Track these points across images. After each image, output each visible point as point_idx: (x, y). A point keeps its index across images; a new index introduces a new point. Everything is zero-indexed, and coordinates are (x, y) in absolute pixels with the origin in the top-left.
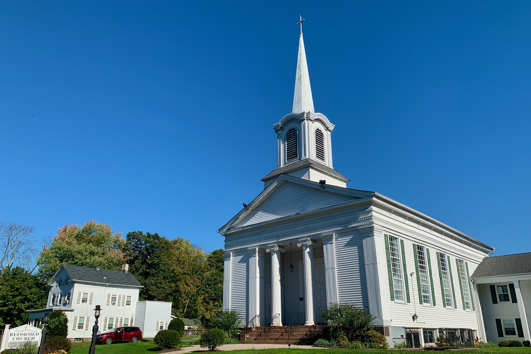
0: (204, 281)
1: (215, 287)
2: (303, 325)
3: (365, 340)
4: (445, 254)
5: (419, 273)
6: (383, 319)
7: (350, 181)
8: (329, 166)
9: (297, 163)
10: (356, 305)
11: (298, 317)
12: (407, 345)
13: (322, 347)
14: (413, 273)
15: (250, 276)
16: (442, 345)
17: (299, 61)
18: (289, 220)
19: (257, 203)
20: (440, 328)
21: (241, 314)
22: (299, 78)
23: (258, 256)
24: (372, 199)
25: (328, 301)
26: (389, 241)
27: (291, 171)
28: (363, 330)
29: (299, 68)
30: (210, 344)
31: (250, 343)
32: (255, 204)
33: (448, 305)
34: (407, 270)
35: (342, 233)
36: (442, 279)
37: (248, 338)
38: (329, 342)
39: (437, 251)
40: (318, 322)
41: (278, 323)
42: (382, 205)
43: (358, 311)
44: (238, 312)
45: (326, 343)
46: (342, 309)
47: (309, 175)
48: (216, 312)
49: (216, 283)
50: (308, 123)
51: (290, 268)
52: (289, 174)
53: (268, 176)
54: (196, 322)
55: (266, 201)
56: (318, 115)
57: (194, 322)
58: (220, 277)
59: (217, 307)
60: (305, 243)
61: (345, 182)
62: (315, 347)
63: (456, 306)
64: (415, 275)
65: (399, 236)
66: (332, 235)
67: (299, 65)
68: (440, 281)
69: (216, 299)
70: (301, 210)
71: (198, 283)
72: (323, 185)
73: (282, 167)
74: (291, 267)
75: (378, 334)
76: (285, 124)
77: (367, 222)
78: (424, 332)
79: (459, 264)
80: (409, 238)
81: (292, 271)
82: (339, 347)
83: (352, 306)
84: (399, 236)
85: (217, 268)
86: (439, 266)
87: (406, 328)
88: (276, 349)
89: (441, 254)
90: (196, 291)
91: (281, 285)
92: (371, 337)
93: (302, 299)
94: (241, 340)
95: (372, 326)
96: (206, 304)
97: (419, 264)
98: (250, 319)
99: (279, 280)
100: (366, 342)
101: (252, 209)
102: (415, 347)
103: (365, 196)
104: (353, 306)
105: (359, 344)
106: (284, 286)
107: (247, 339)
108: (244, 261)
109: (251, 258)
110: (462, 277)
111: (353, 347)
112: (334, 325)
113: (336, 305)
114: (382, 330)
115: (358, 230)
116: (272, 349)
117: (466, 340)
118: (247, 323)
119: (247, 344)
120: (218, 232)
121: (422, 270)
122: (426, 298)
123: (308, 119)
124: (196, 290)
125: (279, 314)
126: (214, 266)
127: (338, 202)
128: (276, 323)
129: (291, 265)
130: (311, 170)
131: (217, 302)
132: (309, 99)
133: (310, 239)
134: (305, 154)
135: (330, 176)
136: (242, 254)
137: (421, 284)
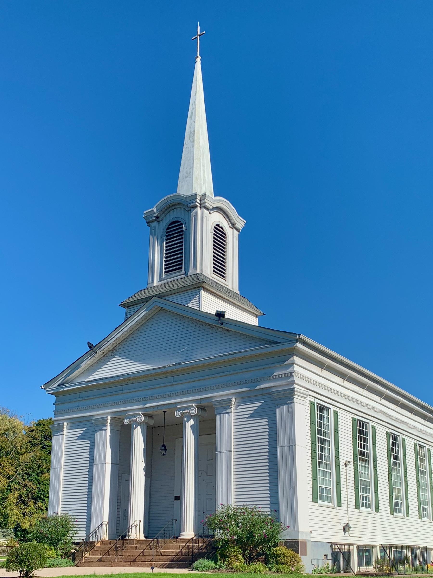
0: (20, 468)
1: (39, 478)
2: (177, 537)
3: (269, 562)
4: (399, 436)
5: (358, 463)
6: (299, 530)
7: (264, 314)
8: (233, 288)
9: (181, 280)
10: (260, 507)
11: (169, 526)
12: (332, 570)
13: (204, 571)
14: (349, 462)
15: (96, 461)
16: (383, 570)
17: (193, 105)
18: (164, 373)
19: (111, 342)
20: (381, 545)
21: (78, 520)
22: (191, 134)
23: (111, 429)
24: (295, 345)
25: (218, 501)
26: (316, 412)
27: (171, 293)
28: (268, 546)
29: (191, 117)
30: (22, 567)
31: (91, 566)
32: (108, 344)
33: (396, 512)
34: (340, 457)
35: (245, 397)
36: (392, 473)
37: (89, 557)
38: (215, 562)
39: (388, 431)
40: (200, 534)
41: (138, 534)
42: (310, 356)
43: (261, 517)
44: (73, 517)
45: (210, 564)
46: (237, 514)
47: (199, 301)
48: (40, 519)
49: (40, 473)
50: (202, 214)
51: (161, 449)
52: (166, 297)
53: (131, 299)
54: (5, 534)
55: (126, 341)
56: (219, 200)
57: (2, 533)
58: (47, 462)
59: (41, 510)
60: (187, 411)
61: (256, 316)
62: (192, 570)
63: (409, 514)
64: (351, 466)
65: (333, 405)
66: (230, 400)
67: (192, 113)
68: (389, 475)
69: (40, 498)
70: (184, 359)
71: (9, 471)
72: (221, 318)
73: (155, 284)
74: (163, 448)
75: (290, 553)
76: (165, 211)
77: (285, 381)
78: (359, 551)
79: (418, 451)
80: (348, 409)
81: (164, 455)
82: (230, 572)
83: (253, 509)
84: (333, 405)
85: (43, 448)
86: (389, 453)
87: (332, 544)
88: (131, 574)
89: (392, 436)
90: (5, 484)
91: (146, 476)
92: (279, 556)
93: (177, 498)
94: (77, 561)
95: (282, 540)
96: (22, 505)
97: (358, 449)
98: (93, 528)
99: (143, 467)
100: (271, 564)
101: (103, 353)
102: (344, 572)
103: (285, 341)
104: (255, 510)
105: (260, 566)
106: (151, 479)
107: (86, 560)
108: (86, 437)
109: (98, 433)
110: (421, 470)
111: (250, 571)
112: (225, 537)
113: (229, 508)
114: (296, 546)
115: (270, 393)
116: (124, 574)
117: (418, 563)
118: (88, 534)
119: (85, 566)
120: (43, 387)
121: (363, 457)
122: (366, 500)
123: (202, 206)
124: (7, 483)
125: (140, 521)
126: (37, 445)
127: (242, 348)
128: (135, 534)
129: (163, 446)
130: (203, 292)
131: (42, 503)
132: (205, 171)
133: (195, 406)
134: (195, 266)
135: (233, 305)
136: (84, 426)
137: (359, 478)
